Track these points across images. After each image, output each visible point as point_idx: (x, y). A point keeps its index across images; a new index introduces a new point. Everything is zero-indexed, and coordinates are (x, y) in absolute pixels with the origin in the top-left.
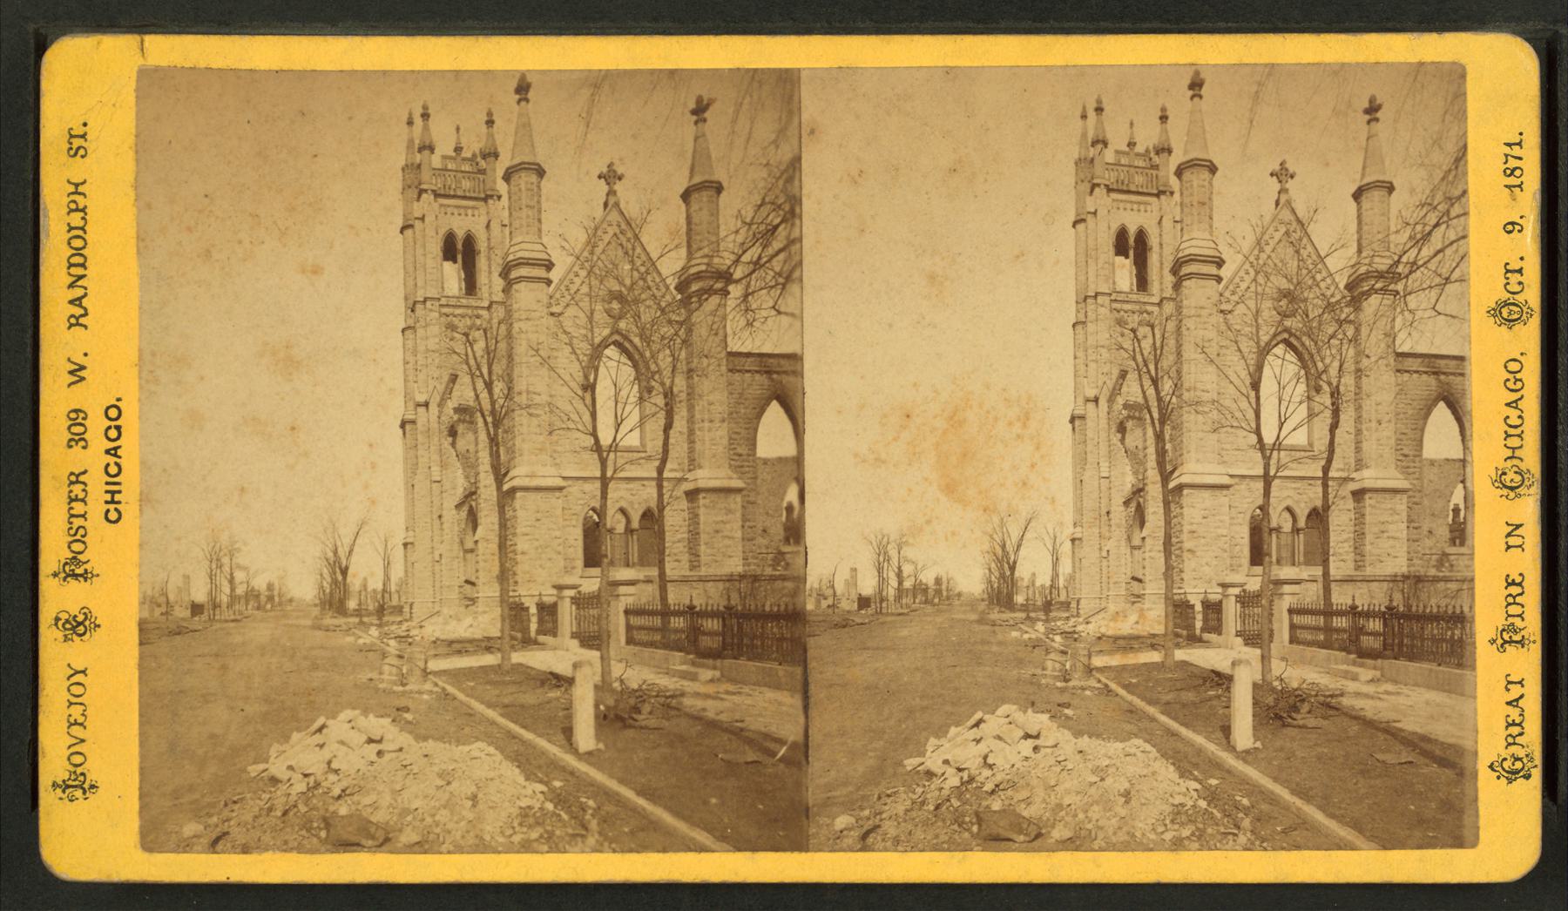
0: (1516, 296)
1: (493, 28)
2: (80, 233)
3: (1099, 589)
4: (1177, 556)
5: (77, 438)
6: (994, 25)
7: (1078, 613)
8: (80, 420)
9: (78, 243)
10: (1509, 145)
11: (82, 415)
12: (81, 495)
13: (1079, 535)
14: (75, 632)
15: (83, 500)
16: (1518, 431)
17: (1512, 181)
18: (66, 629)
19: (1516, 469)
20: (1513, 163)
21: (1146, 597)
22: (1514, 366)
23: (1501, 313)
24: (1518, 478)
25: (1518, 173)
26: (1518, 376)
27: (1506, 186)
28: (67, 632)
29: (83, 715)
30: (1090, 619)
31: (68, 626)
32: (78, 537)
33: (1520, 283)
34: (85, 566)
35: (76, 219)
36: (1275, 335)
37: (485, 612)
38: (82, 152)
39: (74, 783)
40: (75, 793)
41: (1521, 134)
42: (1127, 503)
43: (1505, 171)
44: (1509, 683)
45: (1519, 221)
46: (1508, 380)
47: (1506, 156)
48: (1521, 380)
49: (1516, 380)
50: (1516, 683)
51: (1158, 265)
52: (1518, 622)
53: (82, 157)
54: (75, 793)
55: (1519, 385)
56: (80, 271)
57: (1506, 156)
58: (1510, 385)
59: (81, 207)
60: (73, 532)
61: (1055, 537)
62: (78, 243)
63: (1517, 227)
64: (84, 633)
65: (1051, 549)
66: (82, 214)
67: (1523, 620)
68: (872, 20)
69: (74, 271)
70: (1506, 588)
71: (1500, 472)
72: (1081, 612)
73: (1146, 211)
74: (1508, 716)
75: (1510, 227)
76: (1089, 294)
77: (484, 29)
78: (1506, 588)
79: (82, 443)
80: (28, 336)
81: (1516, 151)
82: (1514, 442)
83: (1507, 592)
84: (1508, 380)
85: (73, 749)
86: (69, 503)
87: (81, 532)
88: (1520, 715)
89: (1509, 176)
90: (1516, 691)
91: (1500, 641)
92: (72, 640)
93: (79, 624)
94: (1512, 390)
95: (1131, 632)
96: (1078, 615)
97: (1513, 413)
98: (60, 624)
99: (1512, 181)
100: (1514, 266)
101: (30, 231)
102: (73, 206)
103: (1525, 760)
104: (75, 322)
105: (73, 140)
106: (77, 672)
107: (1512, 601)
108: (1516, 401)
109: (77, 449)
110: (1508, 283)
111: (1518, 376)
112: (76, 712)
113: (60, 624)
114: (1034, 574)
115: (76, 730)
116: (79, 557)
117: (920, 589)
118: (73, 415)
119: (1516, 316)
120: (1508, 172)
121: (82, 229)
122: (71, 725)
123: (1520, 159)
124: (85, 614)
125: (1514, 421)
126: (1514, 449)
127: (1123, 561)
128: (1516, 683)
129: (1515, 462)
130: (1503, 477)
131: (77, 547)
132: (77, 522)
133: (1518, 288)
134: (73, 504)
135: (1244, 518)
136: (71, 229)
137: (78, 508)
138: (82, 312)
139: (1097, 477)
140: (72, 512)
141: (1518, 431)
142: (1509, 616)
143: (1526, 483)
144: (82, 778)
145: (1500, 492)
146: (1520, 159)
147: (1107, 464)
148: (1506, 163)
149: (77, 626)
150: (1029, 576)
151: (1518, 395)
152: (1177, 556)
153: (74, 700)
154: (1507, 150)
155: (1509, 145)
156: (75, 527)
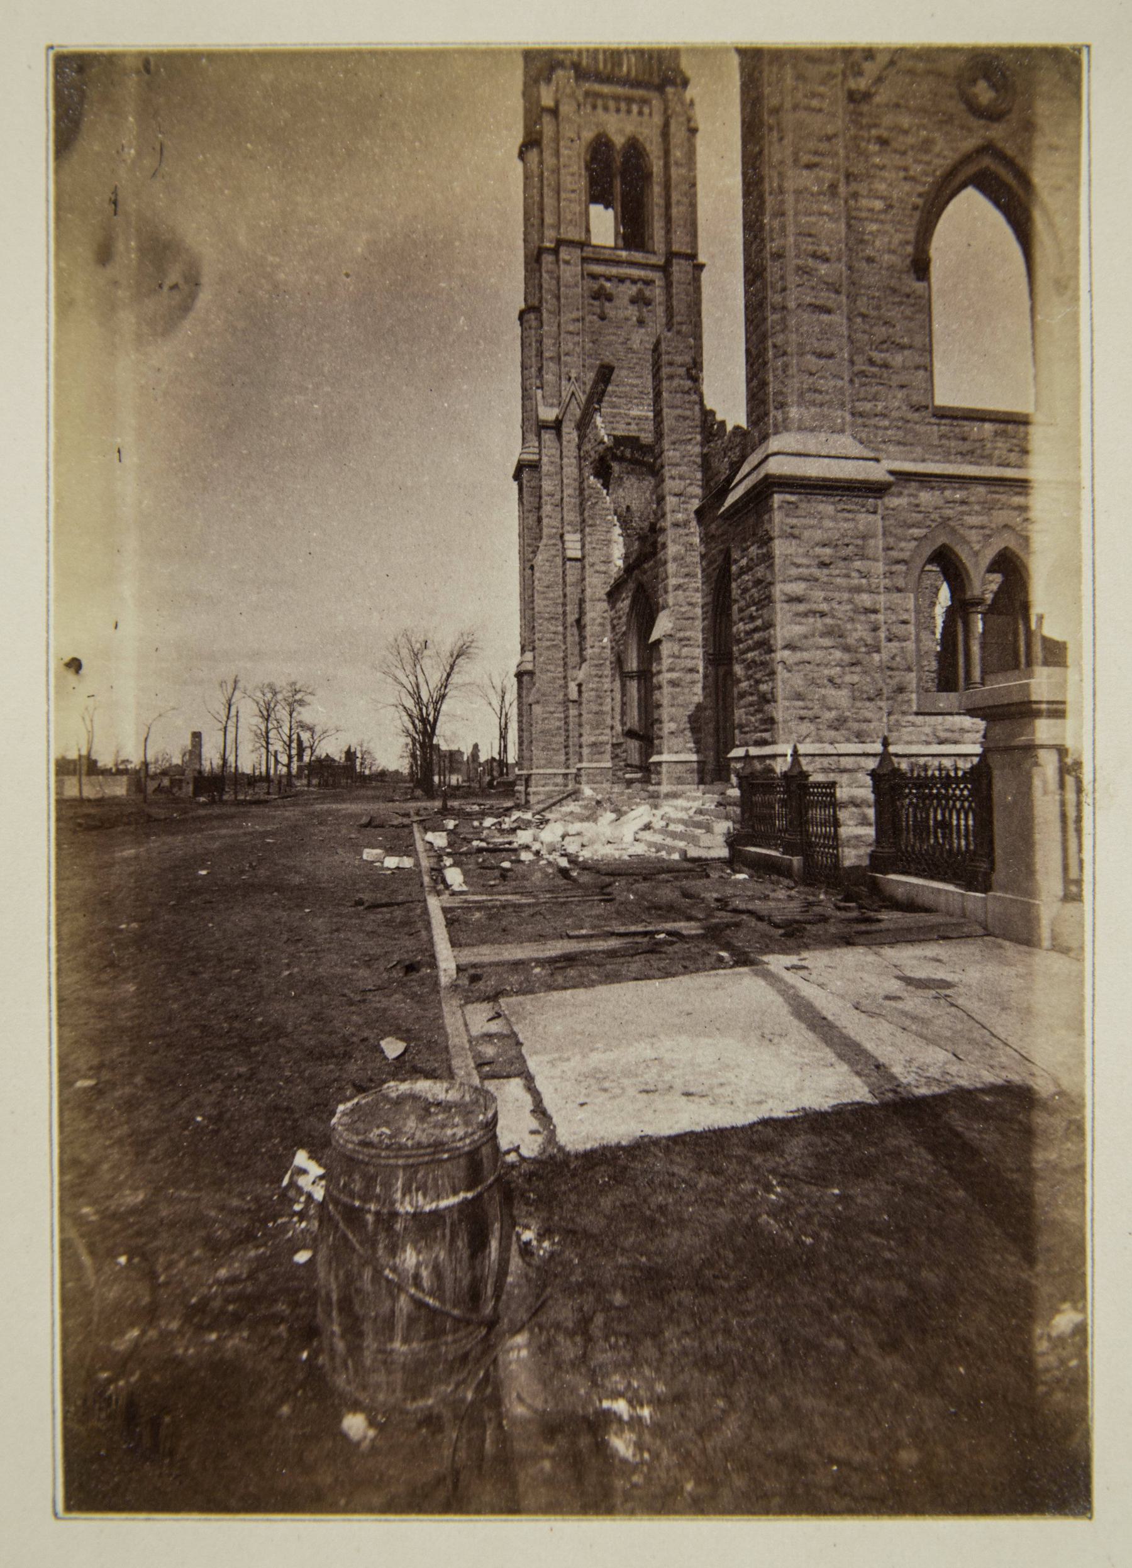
3: (563, 758)
4: (750, 665)
7: (527, 802)
13: (529, 667)
21: (664, 768)
30: (548, 815)
36: (967, 159)
37: (674, 795)
42: (612, 596)
51: (662, 202)
61: (504, 693)
65: (498, 710)
72: (533, 799)
73: (640, 113)
76: (547, 244)
95: (640, 849)
96: (526, 806)
114: (476, 746)
117: (323, 768)
127: (607, 708)
135: (906, 574)
139: (559, 560)
147: (578, 536)
150: (470, 750)
152: (750, 665)
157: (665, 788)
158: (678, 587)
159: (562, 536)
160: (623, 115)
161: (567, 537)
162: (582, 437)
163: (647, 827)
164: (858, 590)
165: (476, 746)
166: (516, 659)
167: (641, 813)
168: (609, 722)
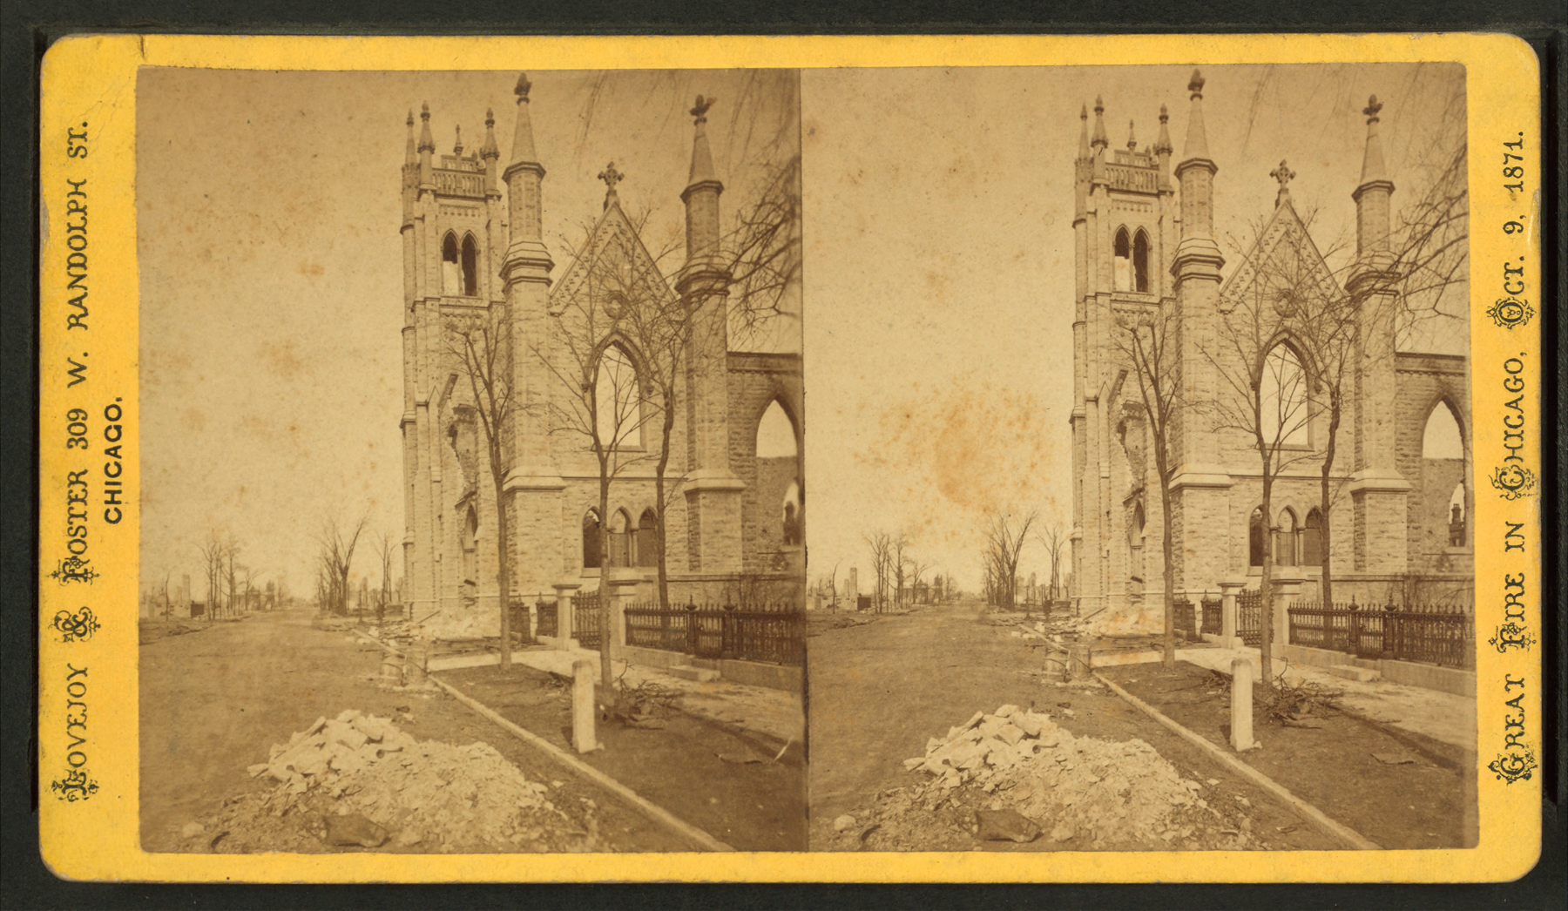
0: (1516, 296)
1: (493, 28)
2: (80, 233)
4: (1177, 556)
5: (77, 438)
6: (994, 25)
7: (1078, 613)
8: (79, 421)
9: (78, 243)
10: (1509, 145)
11: (82, 415)
12: (81, 496)
14: (75, 632)
15: (83, 500)
16: (1518, 431)
17: (1512, 181)
18: (66, 629)
19: (1516, 469)
20: (1513, 163)
22: (1514, 366)
23: (1501, 313)
24: (1518, 478)
25: (1518, 173)
26: (1518, 376)
27: (1506, 186)
28: (67, 632)
29: (83, 715)
31: (68, 626)
32: (78, 537)
33: (1520, 283)
34: (85, 566)
35: (76, 219)
36: (1275, 335)
38: (82, 152)
39: (74, 783)
40: (75, 793)
41: (1521, 134)
42: (1127, 503)
43: (1505, 171)
44: (1509, 683)
45: (1519, 221)
46: (1508, 380)
47: (1506, 156)
48: (1520, 380)
49: (1517, 380)
50: (1515, 683)
51: (1158, 265)
52: (1518, 621)
53: (83, 157)
54: (75, 793)
55: (1519, 385)
56: (80, 271)
57: (1506, 156)
58: (1510, 385)
59: (81, 207)
60: (72, 532)
62: (78, 243)
63: (1517, 228)
64: (84, 634)
66: (82, 214)
67: (1523, 620)
68: (872, 20)
69: (74, 271)
70: (1506, 588)
71: (1500, 472)
72: (1081, 612)
74: (1508, 716)
75: (1510, 228)
77: (484, 28)
78: (1506, 588)
79: (82, 443)
80: (28, 336)
81: (1516, 151)
82: (1514, 442)
83: (1507, 592)
84: (1508, 380)
85: (73, 749)
86: (69, 504)
87: (81, 532)
88: (1520, 715)
89: (1509, 176)
90: (1516, 691)
91: (1500, 641)
92: (72, 640)
93: (80, 624)
94: (1512, 390)
96: (1078, 615)
97: (1513, 413)
98: (60, 623)
99: (1512, 181)
100: (1514, 266)
101: (30, 231)
102: (73, 206)
103: (1525, 760)
104: (75, 322)
105: (72, 140)
106: (77, 672)
107: (1512, 601)
108: (1516, 401)
109: (77, 449)
110: (1508, 283)
111: (1518, 376)
112: (76, 712)
113: (60, 623)
114: (1034, 574)
115: (76, 730)
116: (79, 557)
118: (73, 415)
119: (1516, 316)
120: (1508, 172)
121: (82, 229)
122: (71, 725)
123: (1520, 159)
124: (85, 614)
125: (1514, 421)
126: (1514, 449)
128: (1515, 683)
129: (1515, 462)
130: (1503, 477)
131: (77, 547)
132: (77, 522)
133: (1518, 288)
134: (73, 504)
136: (71, 229)
137: (78, 508)
138: (82, 312)
140: (72, 512)
141: (1518, 431)
142: (1509, 616)
143: (1526, 483)
144: (82, 778)
145: (1500, 492)
146: (1520, 159)
147: (1107, 464)
148: (1505, 163)
149: (77, 626)
151: (1517, 396)
152: (1177, 556)
153: (74, 700)
154: (1507, 150)
155: (1509, 145)
156: (75, 527)
157: (480, 609)
158: (486, 516)
159: (430, 468)
160: (463, 217)
161: (432, 469)
162: (440, 412)
163: (471, 626)
164: (1219, 527)
165: (1034, 574)
166: (403, 534)
167: (468, 620)
168: (1124, 571)
